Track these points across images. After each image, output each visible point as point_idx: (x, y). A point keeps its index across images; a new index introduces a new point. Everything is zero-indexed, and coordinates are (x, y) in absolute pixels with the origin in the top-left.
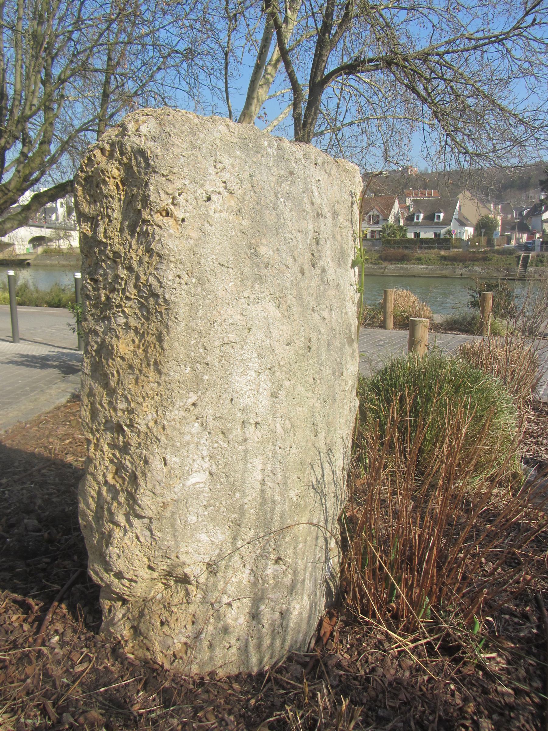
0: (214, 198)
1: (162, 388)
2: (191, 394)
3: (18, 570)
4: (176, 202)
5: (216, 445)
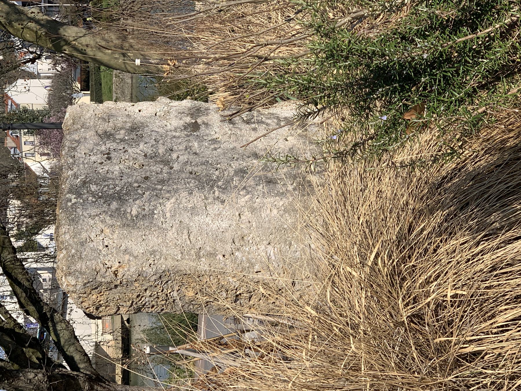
0: (106, 244)
1: (214, 274)
2: (217, 258)
3: (38, 337)
4: (110, 266)
5: (251, 242)
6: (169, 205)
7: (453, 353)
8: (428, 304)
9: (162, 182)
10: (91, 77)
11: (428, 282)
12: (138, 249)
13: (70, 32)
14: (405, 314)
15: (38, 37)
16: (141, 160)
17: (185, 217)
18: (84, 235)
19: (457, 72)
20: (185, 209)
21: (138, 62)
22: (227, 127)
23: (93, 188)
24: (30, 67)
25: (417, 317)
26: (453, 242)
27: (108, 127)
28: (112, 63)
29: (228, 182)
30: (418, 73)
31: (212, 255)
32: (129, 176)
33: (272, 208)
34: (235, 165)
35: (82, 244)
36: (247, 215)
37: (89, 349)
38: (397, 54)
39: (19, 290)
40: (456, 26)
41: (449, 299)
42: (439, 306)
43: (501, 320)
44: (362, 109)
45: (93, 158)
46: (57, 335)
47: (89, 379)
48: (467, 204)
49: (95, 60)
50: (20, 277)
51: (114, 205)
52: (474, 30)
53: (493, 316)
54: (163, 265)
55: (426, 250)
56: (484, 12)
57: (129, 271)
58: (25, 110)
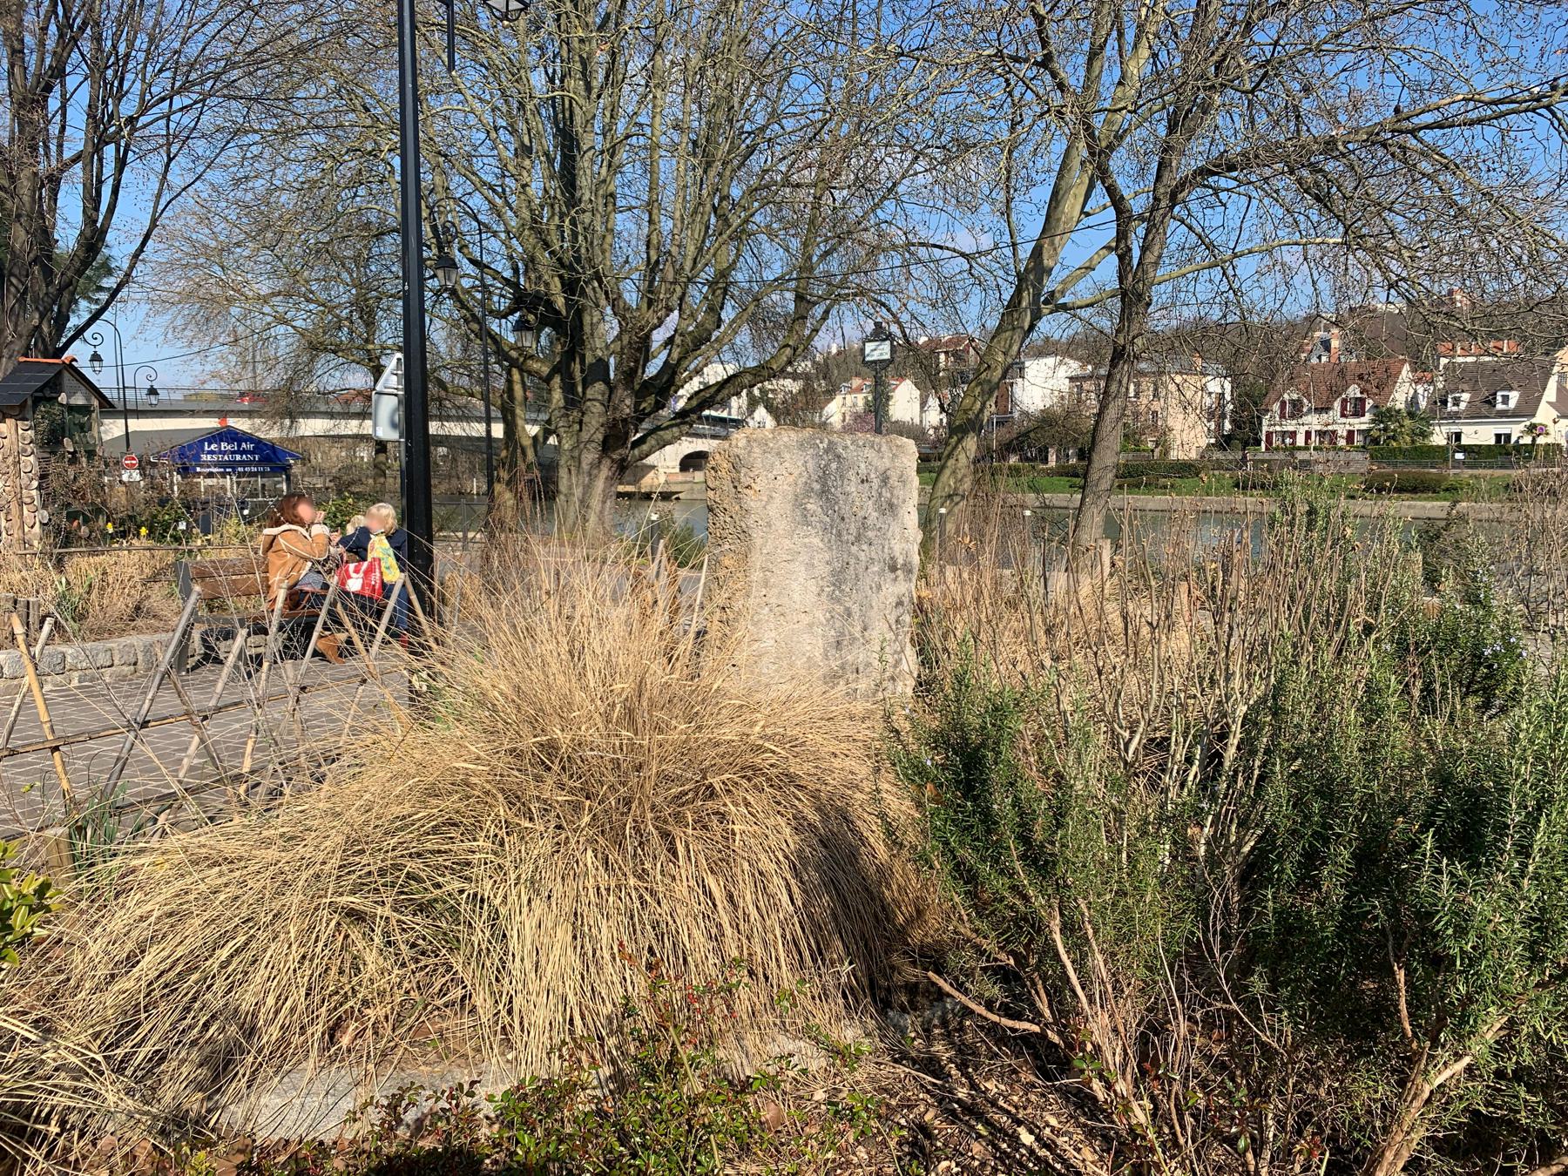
6: (816, 541)
7: (677, 831)
8: (725, 805)
9: (839, 534)
10: (932, 460)
11: (747, 804)
12: (773, 510)
13: (971, 443)
14: (716, 781)
15: (966, 412)
16: (861, 514)
17: (804, 557)
18: (787, 456)
19: (977, 839)
20: (812, 558)
21: (943, 511)
22: (893, 600)
23: (834, 466)
24: (933, 402)
25: (711, 793)
26: (788, 830)
27: (893, 481)
28: (940, 485)
29: (838, 601)
30: (975, 799)
31: (766, 584)
32: (845, 501)
33: (813, 645)
34: (855, 608)
35: (778, 454)
36: (806, 619)
37: (650, 460)
38: (996, 776)
39: (712, 390)
40: (1025, 839)
41: (730, 826)
42: (722, 817)
43: (710, 881)
44: (938, 741)
45: (863, 466)
46: (667, 428)
47: (623, 460)
48: (825, 847)
49: (943, 467)
50: (725, 392)
51: (817, 486)
52: (1020, 858)
53: (712, 872)
54: (757, 535)
55: (779, 803)
56: (1038, 869)
57: (751, 501)
58: (888, 398)
